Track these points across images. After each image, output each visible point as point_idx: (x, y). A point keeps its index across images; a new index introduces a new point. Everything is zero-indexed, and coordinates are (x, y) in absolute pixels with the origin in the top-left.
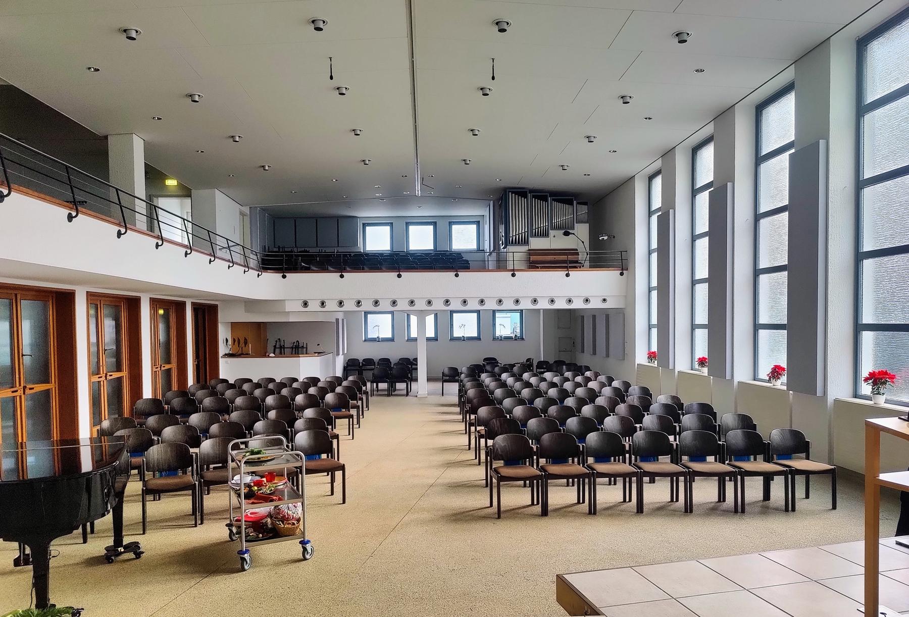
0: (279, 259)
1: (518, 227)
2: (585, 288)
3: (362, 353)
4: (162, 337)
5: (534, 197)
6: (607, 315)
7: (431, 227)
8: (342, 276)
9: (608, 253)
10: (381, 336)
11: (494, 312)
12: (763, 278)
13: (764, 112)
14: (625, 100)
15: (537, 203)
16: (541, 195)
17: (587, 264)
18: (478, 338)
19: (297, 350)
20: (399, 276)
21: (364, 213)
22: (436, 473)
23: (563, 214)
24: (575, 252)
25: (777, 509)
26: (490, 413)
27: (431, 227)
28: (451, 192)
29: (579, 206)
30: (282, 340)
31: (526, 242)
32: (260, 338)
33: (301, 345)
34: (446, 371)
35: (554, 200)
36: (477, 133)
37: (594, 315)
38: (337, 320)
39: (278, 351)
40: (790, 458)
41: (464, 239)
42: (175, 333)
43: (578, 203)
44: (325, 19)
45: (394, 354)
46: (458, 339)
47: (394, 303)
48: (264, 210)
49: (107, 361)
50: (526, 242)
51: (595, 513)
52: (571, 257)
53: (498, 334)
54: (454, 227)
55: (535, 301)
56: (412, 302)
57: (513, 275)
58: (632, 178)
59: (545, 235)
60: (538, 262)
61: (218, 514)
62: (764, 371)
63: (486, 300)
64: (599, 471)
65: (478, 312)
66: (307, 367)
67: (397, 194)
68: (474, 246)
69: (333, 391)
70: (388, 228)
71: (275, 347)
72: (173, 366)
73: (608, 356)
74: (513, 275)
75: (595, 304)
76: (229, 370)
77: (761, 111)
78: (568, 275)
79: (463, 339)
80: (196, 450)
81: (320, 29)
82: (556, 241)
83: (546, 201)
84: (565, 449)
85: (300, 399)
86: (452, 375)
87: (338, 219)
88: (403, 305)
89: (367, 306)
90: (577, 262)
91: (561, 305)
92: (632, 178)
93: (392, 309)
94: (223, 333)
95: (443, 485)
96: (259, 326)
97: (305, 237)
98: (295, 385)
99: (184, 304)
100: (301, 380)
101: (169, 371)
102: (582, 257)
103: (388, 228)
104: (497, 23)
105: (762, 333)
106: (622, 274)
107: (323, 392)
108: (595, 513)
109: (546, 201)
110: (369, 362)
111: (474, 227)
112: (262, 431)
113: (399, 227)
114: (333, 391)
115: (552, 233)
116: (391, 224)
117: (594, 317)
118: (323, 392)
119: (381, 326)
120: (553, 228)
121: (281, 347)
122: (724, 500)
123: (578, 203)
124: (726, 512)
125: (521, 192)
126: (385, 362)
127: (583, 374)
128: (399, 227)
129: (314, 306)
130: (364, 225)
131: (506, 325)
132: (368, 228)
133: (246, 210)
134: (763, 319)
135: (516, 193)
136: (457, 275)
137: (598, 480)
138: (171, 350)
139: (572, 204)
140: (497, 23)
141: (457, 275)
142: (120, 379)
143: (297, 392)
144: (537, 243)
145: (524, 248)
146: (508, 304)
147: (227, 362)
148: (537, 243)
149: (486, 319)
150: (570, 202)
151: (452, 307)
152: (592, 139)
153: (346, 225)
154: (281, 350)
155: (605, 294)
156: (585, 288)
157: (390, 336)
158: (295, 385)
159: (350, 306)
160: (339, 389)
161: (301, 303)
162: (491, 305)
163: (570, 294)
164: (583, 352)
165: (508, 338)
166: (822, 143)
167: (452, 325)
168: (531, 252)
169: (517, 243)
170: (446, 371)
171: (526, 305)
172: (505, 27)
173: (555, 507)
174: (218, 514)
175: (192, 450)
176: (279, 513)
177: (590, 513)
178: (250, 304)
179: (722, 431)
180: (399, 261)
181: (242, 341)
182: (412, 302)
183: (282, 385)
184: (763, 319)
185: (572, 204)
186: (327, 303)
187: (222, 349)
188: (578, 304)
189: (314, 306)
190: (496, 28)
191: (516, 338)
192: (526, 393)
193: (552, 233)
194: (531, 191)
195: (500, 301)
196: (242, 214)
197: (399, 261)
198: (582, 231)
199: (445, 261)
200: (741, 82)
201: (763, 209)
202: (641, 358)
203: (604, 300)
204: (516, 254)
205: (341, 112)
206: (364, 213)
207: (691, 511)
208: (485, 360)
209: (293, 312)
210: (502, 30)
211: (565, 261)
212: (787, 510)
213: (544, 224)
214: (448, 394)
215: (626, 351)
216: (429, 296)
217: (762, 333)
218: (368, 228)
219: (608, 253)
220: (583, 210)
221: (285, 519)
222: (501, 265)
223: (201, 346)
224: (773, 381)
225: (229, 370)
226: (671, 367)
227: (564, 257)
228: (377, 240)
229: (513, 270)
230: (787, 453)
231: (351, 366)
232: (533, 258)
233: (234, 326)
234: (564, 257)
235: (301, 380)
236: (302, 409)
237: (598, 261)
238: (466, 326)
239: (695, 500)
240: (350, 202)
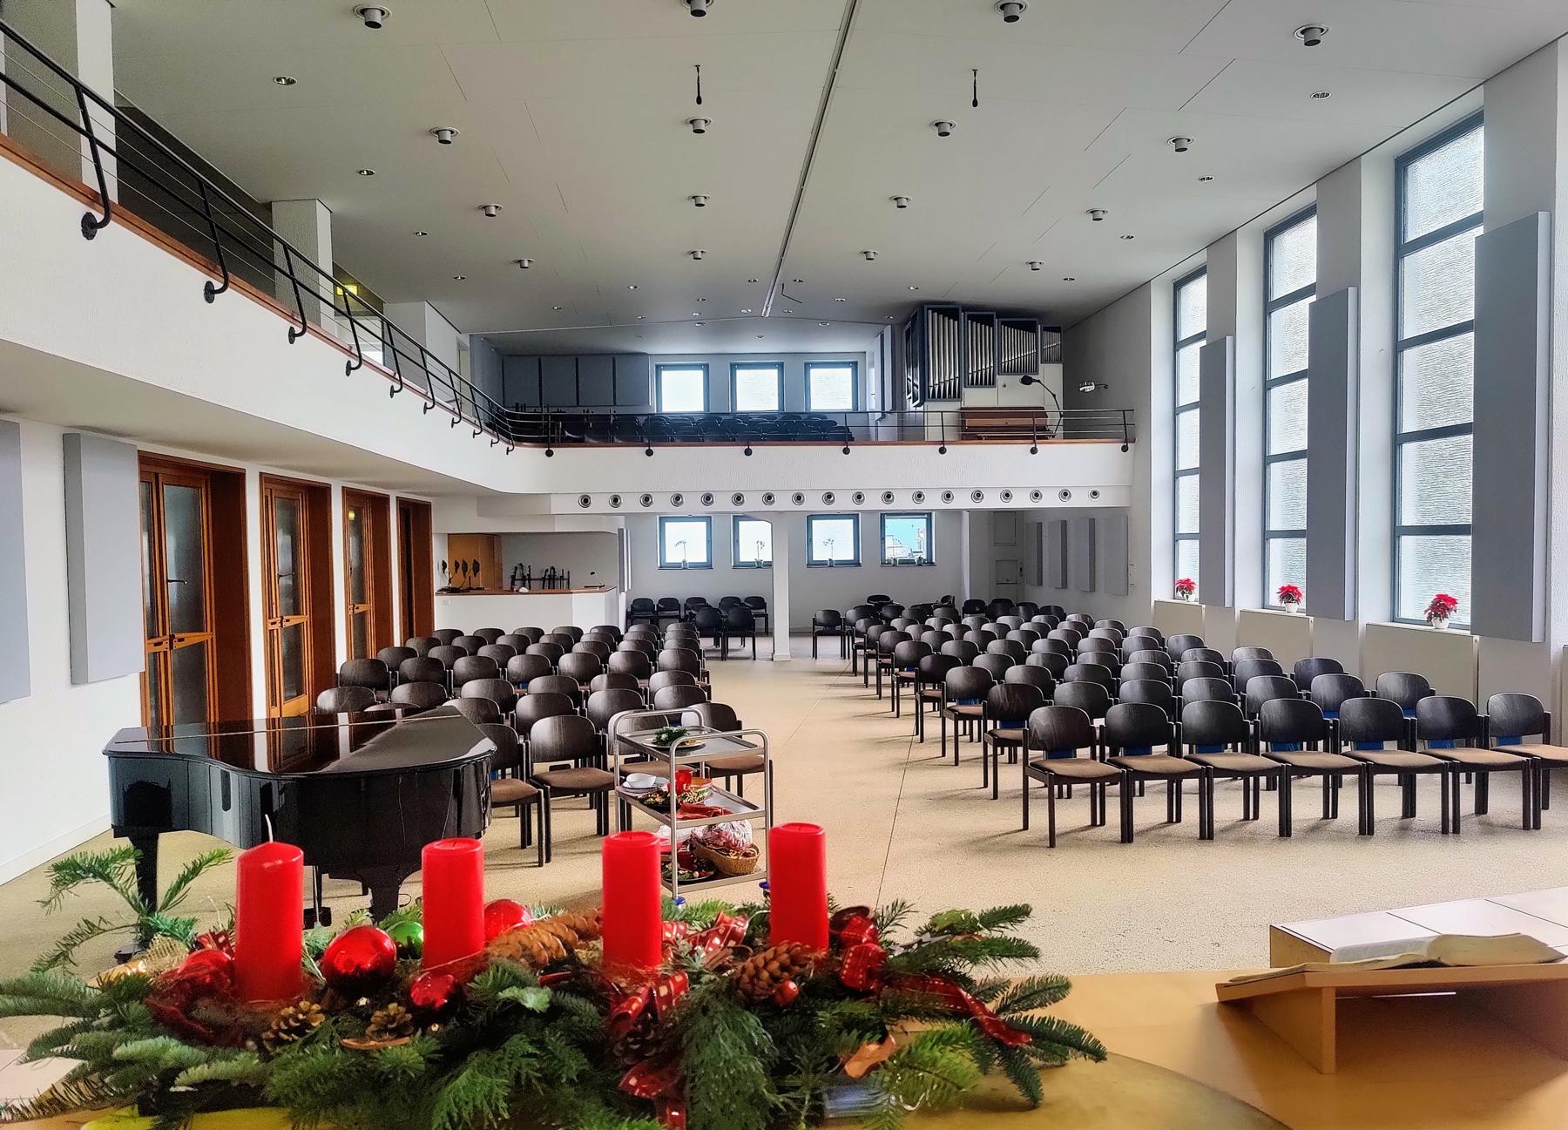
0: (517, 423)
1: (943, 371)
2: (1058, 475)
3: (656, 589)
4: (283, 561)
6: (1090, 520)
7: (849, 371)
8: (748, 452)
10: (689, 560)
11: (883, 516)
12: (1409, 449)
13: (1410, 169)
14: (1180, 146)
15: (975, 328)
16: (982, 315)
17: (1060, 431)
18: (855, 563)
19: (553, 582)
20: (748, 452)
21: (658, 347)
22: (895, 777)
23: (1017, 347)
25: (1508, 827)
26: (967, 677)
27: (849, 371)
29: (1046, 334)
30: (526, 565)
31: (957, 396)
32: (491, 562)
33: (558, 574)
34: (820, 617)
35: (1004, 323)
36: (904, 202)
37: (1064, 522)
38: (621, 531)
40: (1518, 743)
41: (830, 392)
44: (385, 8)
45: (713, 589)
46: (821, 564)
47: (708, 498)
48: (487, 340)
49: (280, 604)
50: (957, 396)
51: (1211, 837)
52: (1038, 421)
53: (889, 555)
54: (814, 372)
55: (978, 495)
56: (677, 498)
57: (942, 451)
58: (1146, 284)
59: (990, 382)
60: (976, 428)
61: (576, 843)
62: (1414, 606)
63: (954, 493)
64: (1219, 765)
65: (854, 516)
66: (587, 611)
67: (721, 311)
68: (848, 406)
69: (522, 652)
70: (774, 373)
71: (513, 578)
73: (1093, 588)
74: (942, 451)
75: (1080, 500)
76: (448, 613)
77: (1405, 169)
78: (1034, 451)
81: (376, 25)
82: (1008, 394)
83: (991, 324)
84: (1307, 724)
85: (461, 665)
86: (832, 624)
87: (614, 357)
88: (723, 503)
89: (662, 505)
90: (1043, 428)
91: (993, 502)
92: (1146, 284)
93: (853, 507)
94: (439, 553)
95: (918, 797)
96: (492, 540)
98: (457, 642)
99: (386, 499)
100: (508, 632)
102: (1054, 420)
103: (700, 374)
104: (1002, 7)
105: (1407, 542)
106: (1125, 449)
107: (507, 652)
108: (1211, 837)
109: (991, 324)
110: (670, 604)
111: (700, 374)
114: (522, 652)
115: (1000, 379)
116: (781, 366)
118: (507, 652)
119: (686, 542)
121: (523, 579)
122: (1335, 816)
123: (1046, 329)
124: (1341, 836)
125: (949, 310)
126: (698, 602)
127: (994, 620)
128: (719, 374)
129: (600, 505)
131: (906, 539)
132: (665, 374)
133: (465, 339)
134: (1275, 524)
135: (940, 311)
137: (1378, 778)
138: (369, 581)
139: (1034, 330)
140: (1002, 7)
142: (297, 627)
143: (459, 652)
144: (975, 398)
145: (954, 406)
147: (445, 603)
148: (975, 398)
149: (870, 527)
150: (1031, 327)
152: (1100, 215)
153: (625, 368)
154: (522, 580)
155: (1094, 484)
156: (1058, 475)
157: (703, 559)
158: (457, 642)
159: (631, 504)
160: (532, 649)
162: (874, 502)
163: (1036, 484)
164: (1040, 583)
165: (906, 563)
166: (1542, 217)
167: (810, 541)
168: (965, 413)
169: (942, 396)
170: (820, 617)
171: (933, 502)
172: (1017, 12)
173: (1223, 825)
174: (576, 843)
176: (719, 837)
177: (1202, 837)
178: (486, 499)
179: (1253, 709)
180: (723, 428)
181: (470, 567)
183: (478, 640)
184: (1275, 524)
185: (1034, 330)
187: (439, 580)
188: (1021, 501)
189: (600, 505)
190: (1001, 15)
191: (921, 563)
192: (902, 648)
193: (1000, 379)
194: (966, 308)
196: (460, 347)
197: (723, 428)
198: (1051, 375)
199: (796, 427)
200: (1375, 117)
201: (1409, 332)
202: (1161, 590)
203: (1095, 493)
204: (938, 415)
205: (636, 168)
206: (658, 347)
207: (1371, 832)
208: (870, 599)
209: (564, 514)
210: (1012, 19)
211: (1024, 427)
212: (1526, 827)
213: (987, 365)
214: (825, 657)
215: (1130, 579)
217: (1407, 542)
218: (665, 374)
220: (1054, 341)
221: (729, 846)
222: (909, 433)
224: (1436, 621)
225: (448, 613)
226: (1228, 604)
227: (1028, 421)
228: (680, 394)
229: (943, 442)
230: (1511, 735)
231: (641, 611)
232: (969, 422)
233: (453, 539)
235: (508, 632)
236: (524, 682)
237: (1077, 428)
238: (833, 541)
239: (1377, 815)
240: (641, 328)
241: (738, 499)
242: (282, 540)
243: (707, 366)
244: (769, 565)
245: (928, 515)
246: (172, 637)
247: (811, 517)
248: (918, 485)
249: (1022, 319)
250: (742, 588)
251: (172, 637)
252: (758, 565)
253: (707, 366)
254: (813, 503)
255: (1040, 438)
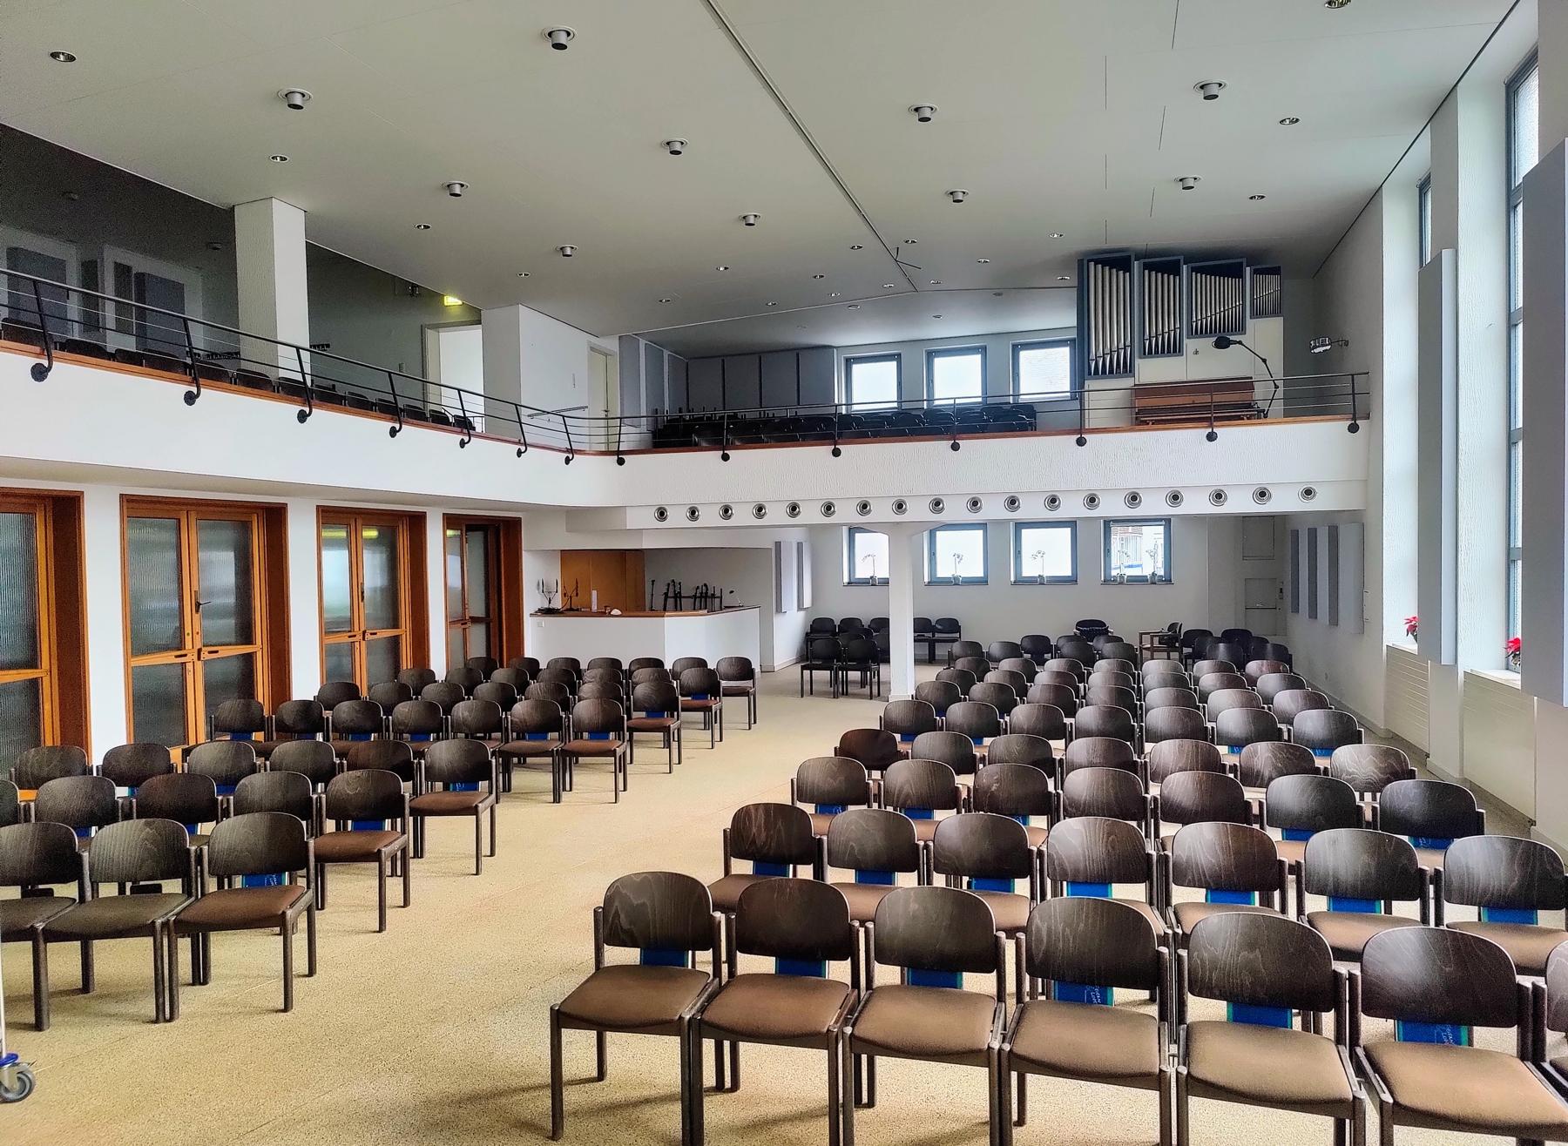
1: (1108, 340)
5: (1147, 266)
9: (1329, 384)
11: (853, 530)
16: (1164, 263)
17: (1278, 406)
18: (1072, 580)
21: (845, 338)
23: (1216, 297)
24: (1246, 385)
27: (977, 358)
28: (1008, 284)
32: (628, 577)
35: (1193, 269)
38: (778, 545)
39: (671, 602)
41: (1045, 374)
42: (408, 572)
43: (1256, 272)
50: (1128, 369)
55: (1219, 496)
57: (1081, 442)
59: (1174, 349)
60: (1155, 410)
65: (1167, 521)
72: (405, 631)
74: (621, 462)
75: (1322, 502)
76: (540, 641)
79: (1038, 581)
80: (1072, 720)
82: (1199, 363)
83: (1177, 273)
87: (798, 352)
88: (919, 511)
90: (1249, 406)
91: (1241, 503)
92: (1373, 199)
93: (1167, 510)
97: (729, 385)
101: (395, 641)
106: (1353, 428)
112: (266, 803)
113: (914, 360)
115: (1189, 344)
117: (1313, 533)
120: (1196, 333)
125: (1118, 261)
128: (997, 354)
129: (678, 518)
130: (849, 362)
131: (1140, 553)
133: (612, 344)
136: (955, 447)
141: (955, 447)
144: (1152, 371)
145: (1128, 382)
146: (956, 510)
147: (539, 625)
148: (1152, 371)
149: (1091, 536)
150: (1235, 272)
151: (1021, 514)
154: (675, 601)
155: (1307, 478)
156: (1275, 464)
161: (653, 512)
168: (1141, 391)
175: (1067, 721)
178: (574, 516)
182: (1053, 500)
186: (701, 512)
187: (531, 600)
188: (1284, 502)
189: (678, 518)
191: (1153, 580)
193: (1189, 344)
194: (1143, 255)
195: (865, 506)
199: (1006, 417)
204: (1106, 396)
206: (845, 338)
215: (1367, 620)
216: (1012, 488)
219: (1329, 384)
223: (493, 592)
225: (540, 641)
228: (873, 387)
234: (1206, 399)
238: (1048, 554)
241: (1134, 498)
242: (454, 562)
243: (984, 348)
244: (885, 582)
245: (1071, 524)
246: (199, 651)
247: (1108, 523)
248: (1052, 487)
249: (1221, 263)
250: (861, 608)
251: (199, 651)
252: (870, 582)
253: (984, 348)
254: (1113, 506)
255: (1217, 419)
